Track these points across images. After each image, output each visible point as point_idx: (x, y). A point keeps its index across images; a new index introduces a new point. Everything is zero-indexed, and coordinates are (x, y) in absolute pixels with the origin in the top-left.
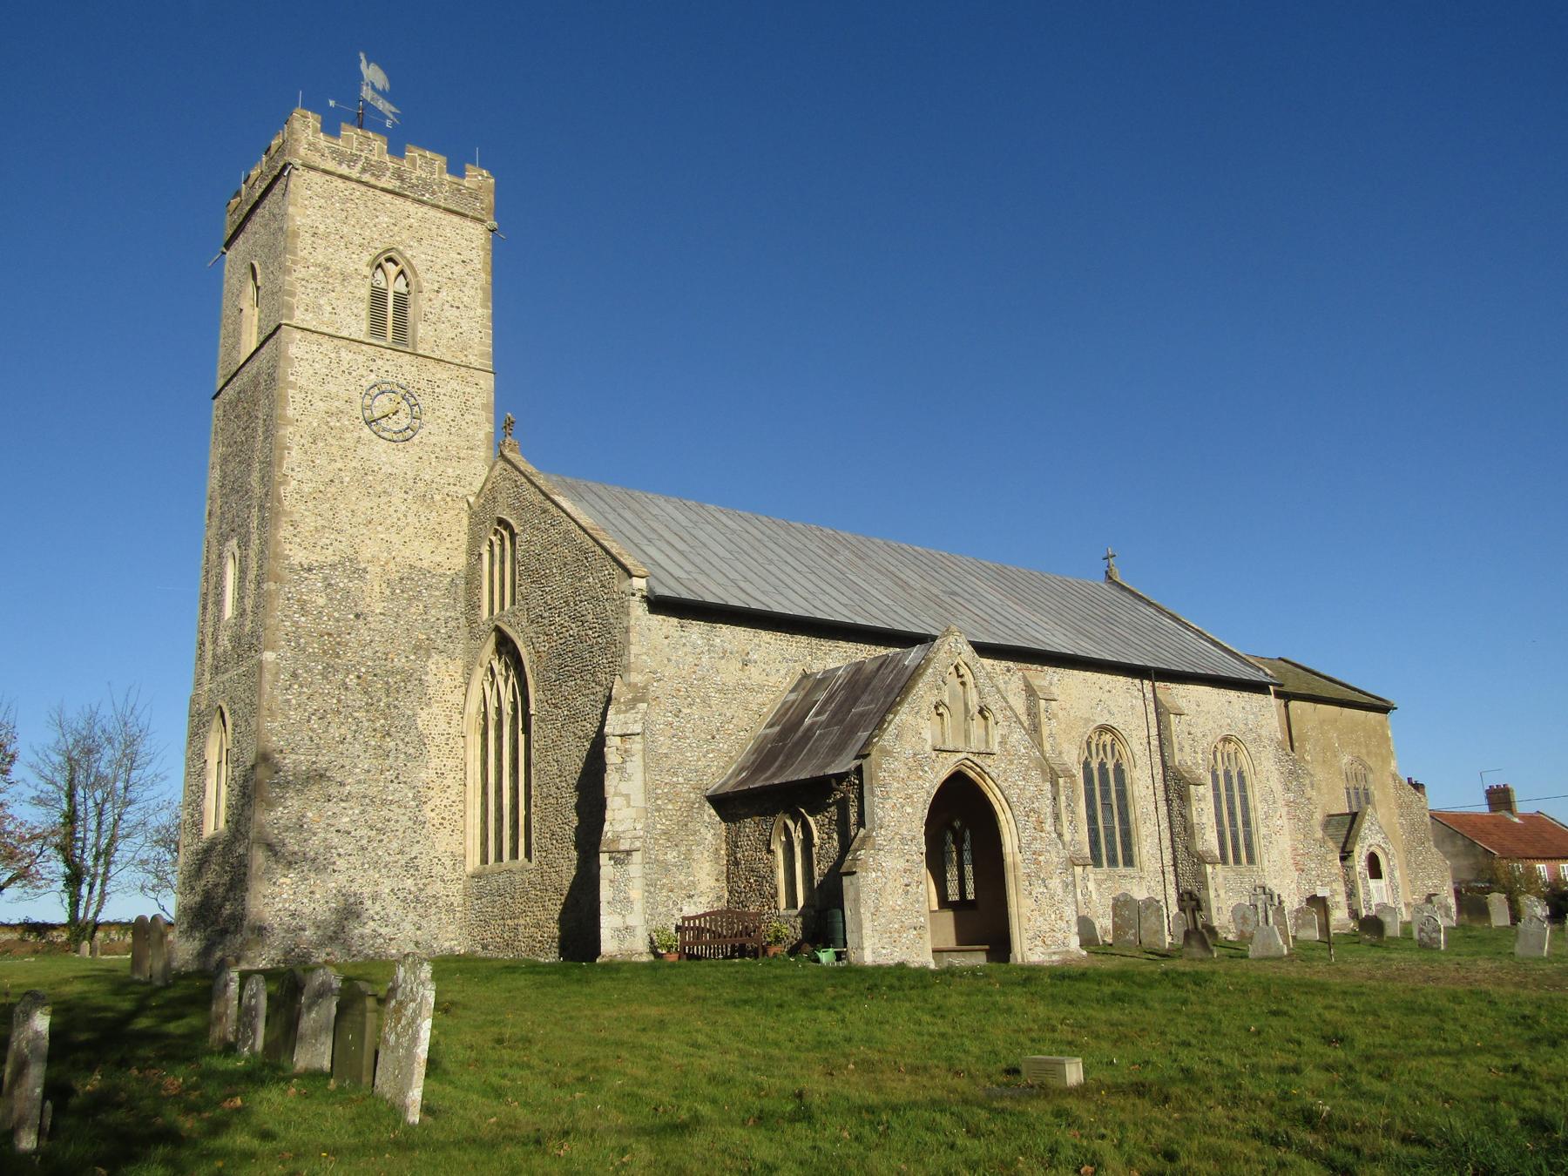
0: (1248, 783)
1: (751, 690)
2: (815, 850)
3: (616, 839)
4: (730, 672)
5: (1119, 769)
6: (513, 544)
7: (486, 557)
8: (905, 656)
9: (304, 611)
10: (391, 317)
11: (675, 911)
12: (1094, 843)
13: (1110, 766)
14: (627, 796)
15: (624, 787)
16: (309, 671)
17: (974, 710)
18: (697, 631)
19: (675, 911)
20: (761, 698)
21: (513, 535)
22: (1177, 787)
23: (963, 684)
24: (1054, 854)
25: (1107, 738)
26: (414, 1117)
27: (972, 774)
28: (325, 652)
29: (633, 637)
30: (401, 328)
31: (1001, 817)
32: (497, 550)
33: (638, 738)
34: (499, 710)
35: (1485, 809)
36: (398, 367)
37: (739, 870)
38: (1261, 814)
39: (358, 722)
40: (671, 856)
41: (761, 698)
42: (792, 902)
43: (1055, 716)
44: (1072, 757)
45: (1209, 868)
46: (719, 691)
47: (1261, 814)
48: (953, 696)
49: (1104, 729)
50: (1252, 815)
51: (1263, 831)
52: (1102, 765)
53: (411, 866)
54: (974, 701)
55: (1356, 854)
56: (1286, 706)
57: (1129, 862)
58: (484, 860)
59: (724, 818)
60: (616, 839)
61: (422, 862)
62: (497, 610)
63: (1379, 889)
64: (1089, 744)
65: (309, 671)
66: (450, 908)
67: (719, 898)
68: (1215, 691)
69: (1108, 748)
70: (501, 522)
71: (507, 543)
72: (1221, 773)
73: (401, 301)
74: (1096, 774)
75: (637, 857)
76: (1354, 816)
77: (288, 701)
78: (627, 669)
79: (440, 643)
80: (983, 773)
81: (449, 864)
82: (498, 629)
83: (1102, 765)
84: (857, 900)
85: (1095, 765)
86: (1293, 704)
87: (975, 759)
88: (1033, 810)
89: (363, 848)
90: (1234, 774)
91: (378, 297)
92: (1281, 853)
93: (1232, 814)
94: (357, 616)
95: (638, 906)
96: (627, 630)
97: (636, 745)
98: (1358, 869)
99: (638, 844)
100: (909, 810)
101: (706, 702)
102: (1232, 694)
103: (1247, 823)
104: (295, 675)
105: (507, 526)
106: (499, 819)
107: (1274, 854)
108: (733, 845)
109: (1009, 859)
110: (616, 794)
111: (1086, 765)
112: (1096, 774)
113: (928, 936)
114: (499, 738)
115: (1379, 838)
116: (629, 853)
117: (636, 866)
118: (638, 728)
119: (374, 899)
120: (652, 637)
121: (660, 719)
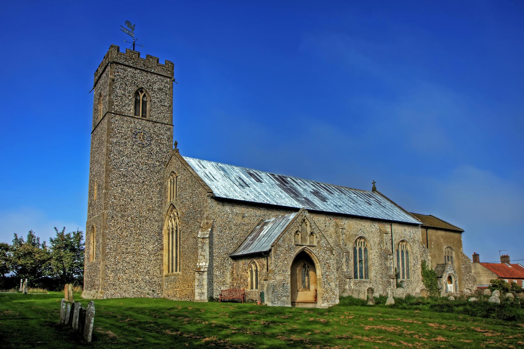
1: (245, 225)
2: (258, 273)
4: (239, 220)
7: (169, 182)
8: (289, 216)
9: (115, 199)
11: (219, 289)
12: (356, 272)
14: (204, 256)
15: (203, 253)
17: (309, 233)
18: (228, 208)
19: (219, 289)
24: (333, 276)
25: (363, 240)
26: (90, 339)
27: (307, 252)
28: (121, 211)
30: (144, 115)
33: (207, 239)
34: (172, 229)
35: (500, 263)
36: (139, 124)
39: (132, 231)
45: (392, 280)
46: (235, 225)
51: (412, 269)
52: (360, 249)
54: (309, 230)
55: (444, 277)
57: (367, 276)
58: (169, 272)
61: (151, 272)
63: (451, 287)
69: (363, 244)
70: (173, 172)
74: (358, 251)
77: (111, 225)
79: (156, 208)
81: (159, 272)
83: (360, 249)
86: (430, 231)
88: (327, 263)
89: (133, 267)
92: (418, 276)
94: (131, 200)
95: (206, 287)
100: (286, 262)
101: (230, 229)
103: (408, 266)
104: (113, 217)
110: (201, 255)
111: (355, 249)
112: (358, 251)
114: (173, 237)
115: (452, 272)
116: (203, 272)
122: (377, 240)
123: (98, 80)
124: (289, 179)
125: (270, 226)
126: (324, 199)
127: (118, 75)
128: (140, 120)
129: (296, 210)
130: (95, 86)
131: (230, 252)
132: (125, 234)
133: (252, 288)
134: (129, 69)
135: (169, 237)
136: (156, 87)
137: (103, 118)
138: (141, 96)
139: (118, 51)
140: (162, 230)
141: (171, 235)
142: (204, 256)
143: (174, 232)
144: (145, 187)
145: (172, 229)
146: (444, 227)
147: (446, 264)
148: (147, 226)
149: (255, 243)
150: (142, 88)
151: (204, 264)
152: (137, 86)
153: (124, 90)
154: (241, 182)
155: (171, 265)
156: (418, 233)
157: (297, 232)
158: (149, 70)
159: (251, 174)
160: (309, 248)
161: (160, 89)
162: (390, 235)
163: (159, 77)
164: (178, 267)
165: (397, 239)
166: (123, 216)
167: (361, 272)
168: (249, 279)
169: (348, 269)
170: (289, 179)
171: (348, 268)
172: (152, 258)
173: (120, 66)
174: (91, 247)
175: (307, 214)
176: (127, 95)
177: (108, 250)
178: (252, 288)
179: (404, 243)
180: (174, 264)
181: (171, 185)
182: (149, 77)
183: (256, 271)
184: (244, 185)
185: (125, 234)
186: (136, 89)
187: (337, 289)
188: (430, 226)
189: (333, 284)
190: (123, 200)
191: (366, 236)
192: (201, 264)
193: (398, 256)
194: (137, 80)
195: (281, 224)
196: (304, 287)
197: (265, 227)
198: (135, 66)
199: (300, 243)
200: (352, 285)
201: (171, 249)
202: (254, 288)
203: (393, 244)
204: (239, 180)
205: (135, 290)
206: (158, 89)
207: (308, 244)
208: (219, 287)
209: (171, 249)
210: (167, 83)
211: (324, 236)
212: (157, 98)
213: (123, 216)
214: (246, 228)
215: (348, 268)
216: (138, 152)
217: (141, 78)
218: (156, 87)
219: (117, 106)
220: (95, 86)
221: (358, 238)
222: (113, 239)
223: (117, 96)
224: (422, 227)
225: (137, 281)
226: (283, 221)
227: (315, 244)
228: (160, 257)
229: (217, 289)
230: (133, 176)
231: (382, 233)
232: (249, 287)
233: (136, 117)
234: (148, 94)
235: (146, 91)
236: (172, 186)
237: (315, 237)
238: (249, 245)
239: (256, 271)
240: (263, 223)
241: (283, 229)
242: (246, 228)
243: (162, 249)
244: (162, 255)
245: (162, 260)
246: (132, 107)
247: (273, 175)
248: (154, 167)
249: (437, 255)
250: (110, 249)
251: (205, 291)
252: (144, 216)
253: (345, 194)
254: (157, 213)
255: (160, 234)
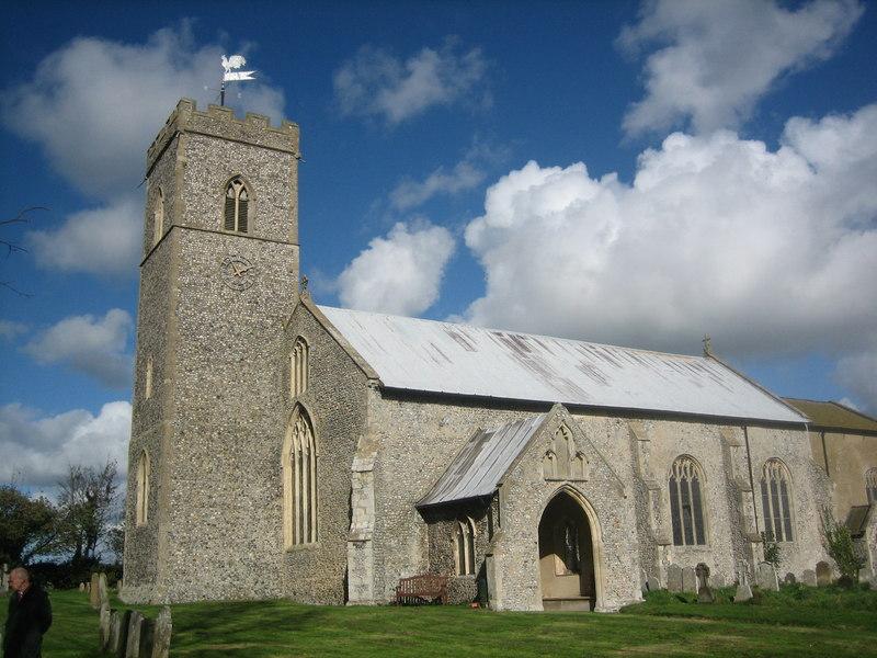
0: (788, 488)
2: (475, 540)
3: (356, 534)
4: (432, 432)
5: (695, 483)
6: (307, 349)
7: (293, 359)
8: (532, 419)
10: (237, 216)
13: (689, 480)
14: (365, 508)
15: (362, 503)
16: (190, 430)
17: (573, 454)
18: (409, 408)
20: (451, 446)
21: (307, 348)
22: (735, 492)
23: (566, 438)
25: (688, 463)
27: (571, 494)
29: (370, 411)
30: (243, 228)
31: (591, 520)
32: (299, 355)
34: (301, 452)
36: (236, 245)
37: (436, 553)
38: (796, 509)
40: (393, 543)
41: (451, 446)
42: (472, 572)
43: (649, 450)
44: (661, 478)
45: (754, 545)
47: (796, 509)
48: (559, 447)
49: (684, 457)
50: (791, 509)
51: (798, 519)
52: (684, 480)
53: (252, 545)
54: (573, 450)
55: (868, 533)
56: (823, 437)
57: (701, 541)
58: (294, 543)
59: (426, 521)
60: (356, 534)
61: (258, 543)
62: (299, 392)
64: (674, 467)
65: (190, 430)
66: (275, 570)
67: (424, 568)
68: (764, 430)
69: (688, 472)
70: (300, 338)
71: (304, 351)
72: (768, 482)
73: (244, 205)
74: (679, 486)
75: (369, 544)
76: (870, 506)
78: (367, 430)
80: (578, 493)
81: (274, 544)
82: (298, 403)
83: (684, 480)
84: (493, 570)
85: (678, 480)
86: (827, 435)
87: (573, 484)
89: (223, 535)
90: (778, 483)
91: (230, 203)
93: (777, 514)
94: (218, 397)
95: (370, 573)
96: (366, 407)
97: (370, 478)
98: (869, 542)
99: (370, 536)
100: (528, 516)
101: (416, 449)
102: (777, 432)
103: (787, 514)
104: (182, 433)
105: (304, 341)
106: (302, 519)
107: (806, 534)
108: (432, 536)
109: (595, 545)
113: (539, 592)
114: (301, 475)
116: (364, 541)
117: (368, 549)
118: (370, 467)
119: (230, 564)
120: (381, 413)
121: (387, 461)
122: (718, 460)
123: (154, 164)
124: (531, 342)
125: (494, 441)
126: (602, 380)
127: (194, 155)
128: (236, 238)
129: (544, 407)
130: (148, 175)
131: (417, 497)
132: (206, 466)
133: (463, 572)
134: (214, 142)
135: (294, 470)
136: (265, 172)
137: (163, 238)
138: (238, 188)
139: (194, 108)
140: (279, 455)
141: (297, 466)
142: (365, 508)
143: (299, 459)
144: (246, 369)
145: (301, 452)
146: (859, 427)
147: (870, 506)
148: (249, 449)
149: (467, 477)
150: (238, 176)
151: (365, 524)
152: (230, 173)
153: (205, 181)
154: (436, 353)
155: (298, 528)
156: (804, 443)
157: (547, 453)
158: (251, 141)
159: (454, 336)
160: (573, 484)
161: (272, 176)
162: (745, 448)
163: (271, 153)
164: (313, 532)
165: (759, 457)
166: (203, 429)
167: (689, 526)
168: (457, 553)
169: (663, 523)
170: (531, 342)
171: (660, 523)
172: (261, 514)
173: (197, 138)
174: (140, 495)
175: (566, 415)
176: (210, 190)
177: (173, 502)
178: (463, 572)
179: (776, 466)
180: (306, 526)
181: (296, 365)
182: (253, 154)
183: (471, 536)
184: (441, 358)
185: (206, 466)
186: (228, 178)
187: (637, 568)
188: (828, 425)
189: (626, 559)
190: (202, 398)
191: (694, 452)
192: (358, 526)
193: (764, 491)
194: (228, 162)
195: (517, 437)
196: (148, 627)
197: (486, 445)
198: (226, 136)
199: (555, 477)
200: (669, 558)
201: (297, 495)
202: (468, 572)
203: (753, 467)
204: (430, 349)
205: (227, 583)
206: (268, 175)
207: (573, 477)
208: (396, 571)
209: (297, 495)
210: (285, 163)
211: (603, 459)
212: (268, 194)
213: (203, 429)
214: (447, 448)
215: (660, 523)
216: (232, 300)
217: (239, 158)
218: (265, 172)
219: (191, 212)
220: (148, 175)
221: (678, 458)
222: (182, 478)
223: (191, 195)
224: (812, 428)
225: (230, 564)
226: (521, 432)
227: (587, 477)
228: (276, 512)
229: (392, 577)
230: (222, 350)
231: (726, 445)
232: (458, 571)
233: (228, 232)
234: (250, 187)
235: (247, 182)
236: (299, 366)
237: (585, 461)
238: (449, 487)
239: (471, 536)
240: (481, 438)
241: (521, 447)
242: (447, 448)
243: (280, 495)
244: (280, 508)
245: (280, 518)
246: (220, 214)
247: (499, 334)
248: (264, 327)
249: (850, 487)
250: (178, 498)
251: (368, 581)
252: (244, 429)
253: (647, 367)
254: (269, 421)
255: (275, 463)
